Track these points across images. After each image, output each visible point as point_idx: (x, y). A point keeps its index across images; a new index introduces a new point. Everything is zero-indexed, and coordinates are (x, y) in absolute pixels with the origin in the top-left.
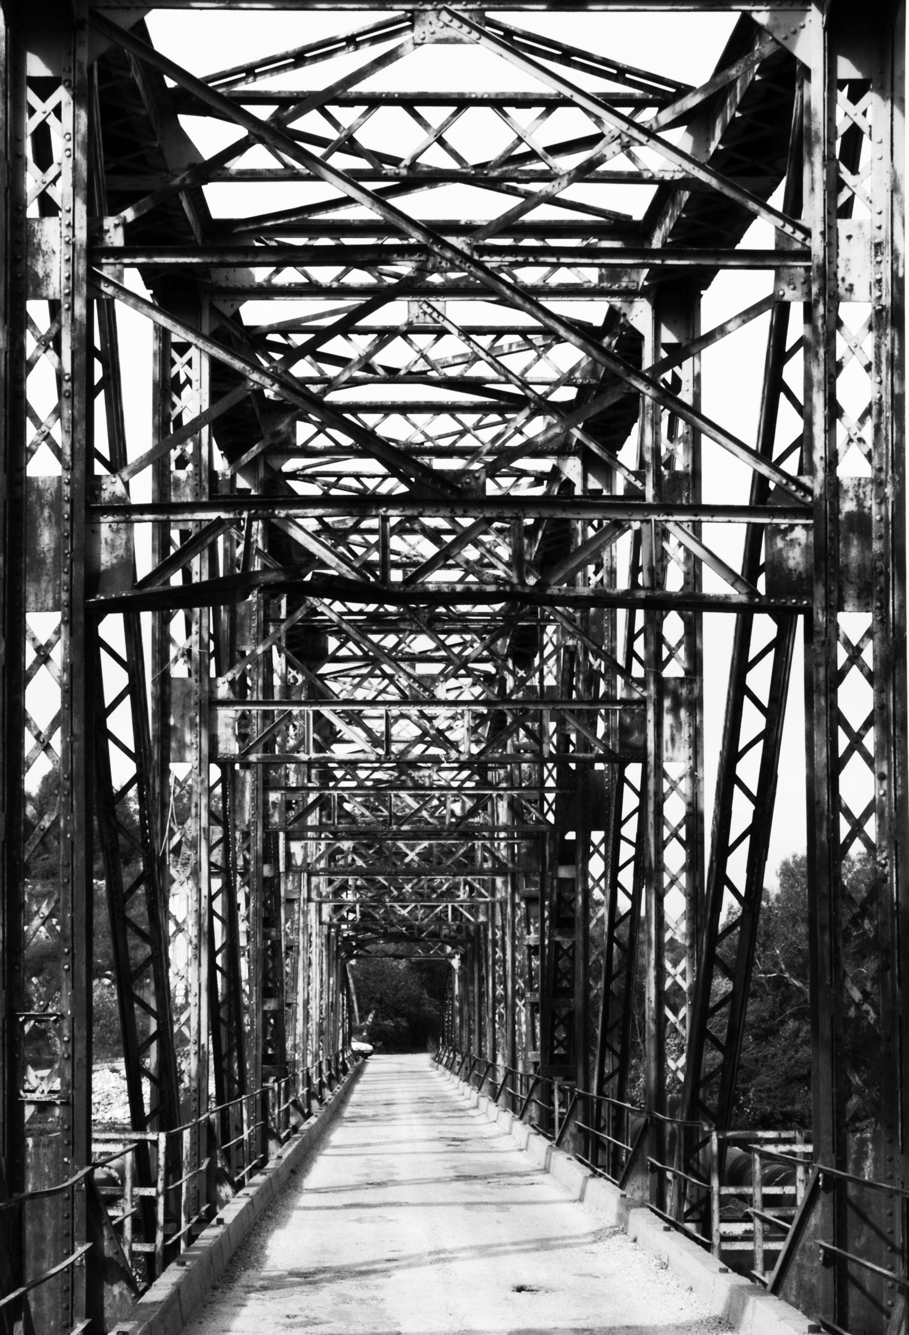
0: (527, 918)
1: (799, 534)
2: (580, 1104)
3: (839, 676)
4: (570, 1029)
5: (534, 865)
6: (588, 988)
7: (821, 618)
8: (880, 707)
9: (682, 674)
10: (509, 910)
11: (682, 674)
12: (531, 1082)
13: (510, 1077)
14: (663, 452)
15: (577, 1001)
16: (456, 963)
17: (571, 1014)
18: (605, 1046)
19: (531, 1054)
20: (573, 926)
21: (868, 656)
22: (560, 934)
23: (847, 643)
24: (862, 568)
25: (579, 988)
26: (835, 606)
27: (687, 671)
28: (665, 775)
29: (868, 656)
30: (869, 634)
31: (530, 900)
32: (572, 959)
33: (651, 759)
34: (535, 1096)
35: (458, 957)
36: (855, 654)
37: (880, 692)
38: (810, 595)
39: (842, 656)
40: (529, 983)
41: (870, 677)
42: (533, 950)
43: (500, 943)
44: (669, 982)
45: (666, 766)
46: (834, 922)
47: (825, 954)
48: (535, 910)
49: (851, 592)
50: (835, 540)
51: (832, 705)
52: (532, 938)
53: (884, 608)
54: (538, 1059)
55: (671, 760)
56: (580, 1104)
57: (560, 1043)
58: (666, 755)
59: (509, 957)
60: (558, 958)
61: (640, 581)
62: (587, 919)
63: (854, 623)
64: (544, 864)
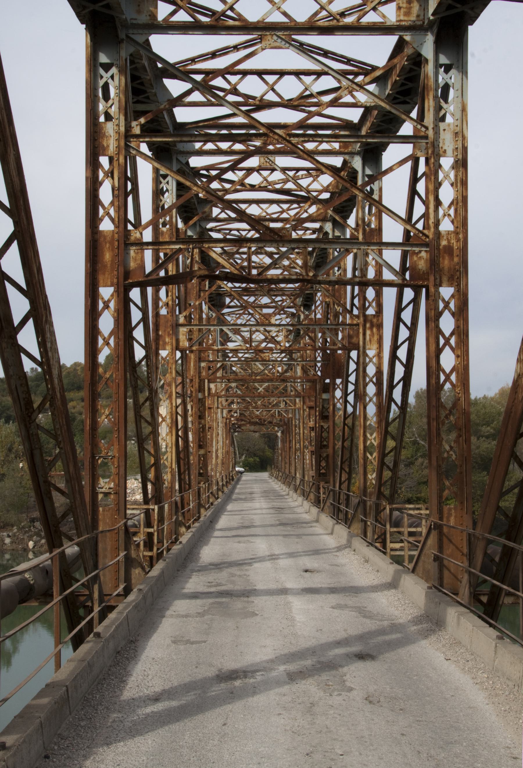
0: (309, 415)
1: (423, 254)
2: (331, 493)
3: (440, 314)
4: (327, 462)
6: (334, 445)
8: (457, 327)
9: (374, 313)
11: (374, 313)
12: (311, 484)
14: (366, 220)
15: (330, 450)
16: (279, 434)
17: (328, 456)
18: (342, 469)
19: (311, 472)
20: (328, 419)
21: (452, 305)
22: (323, 422)
23: (443, 300)
24: (450, 269)
25: (331, 445)
27: (376, 312)
29: (452, 305)
30: (453, 296)
31: (310, 408)
32: (328, 432)
34: (312, 490)
36: (447, 305)
37: (457, 321)
38: (428, 279)
39: (441, 305)
41: (453, 314)
42: (312, 429)
44: (368, 442)
45: (368, 352)
46: (438, 417)
48: (313, 412)
49: (445, 279)
51: (437, 326)
52: (312, 424)
53: (459, 285)
54: (314, 475)
55: (370, 349)
56: (331, 493)
57: (323, 468)
58: (367, 347)
60: (322, 432)
62: (334, 415)
64: (316, 393)
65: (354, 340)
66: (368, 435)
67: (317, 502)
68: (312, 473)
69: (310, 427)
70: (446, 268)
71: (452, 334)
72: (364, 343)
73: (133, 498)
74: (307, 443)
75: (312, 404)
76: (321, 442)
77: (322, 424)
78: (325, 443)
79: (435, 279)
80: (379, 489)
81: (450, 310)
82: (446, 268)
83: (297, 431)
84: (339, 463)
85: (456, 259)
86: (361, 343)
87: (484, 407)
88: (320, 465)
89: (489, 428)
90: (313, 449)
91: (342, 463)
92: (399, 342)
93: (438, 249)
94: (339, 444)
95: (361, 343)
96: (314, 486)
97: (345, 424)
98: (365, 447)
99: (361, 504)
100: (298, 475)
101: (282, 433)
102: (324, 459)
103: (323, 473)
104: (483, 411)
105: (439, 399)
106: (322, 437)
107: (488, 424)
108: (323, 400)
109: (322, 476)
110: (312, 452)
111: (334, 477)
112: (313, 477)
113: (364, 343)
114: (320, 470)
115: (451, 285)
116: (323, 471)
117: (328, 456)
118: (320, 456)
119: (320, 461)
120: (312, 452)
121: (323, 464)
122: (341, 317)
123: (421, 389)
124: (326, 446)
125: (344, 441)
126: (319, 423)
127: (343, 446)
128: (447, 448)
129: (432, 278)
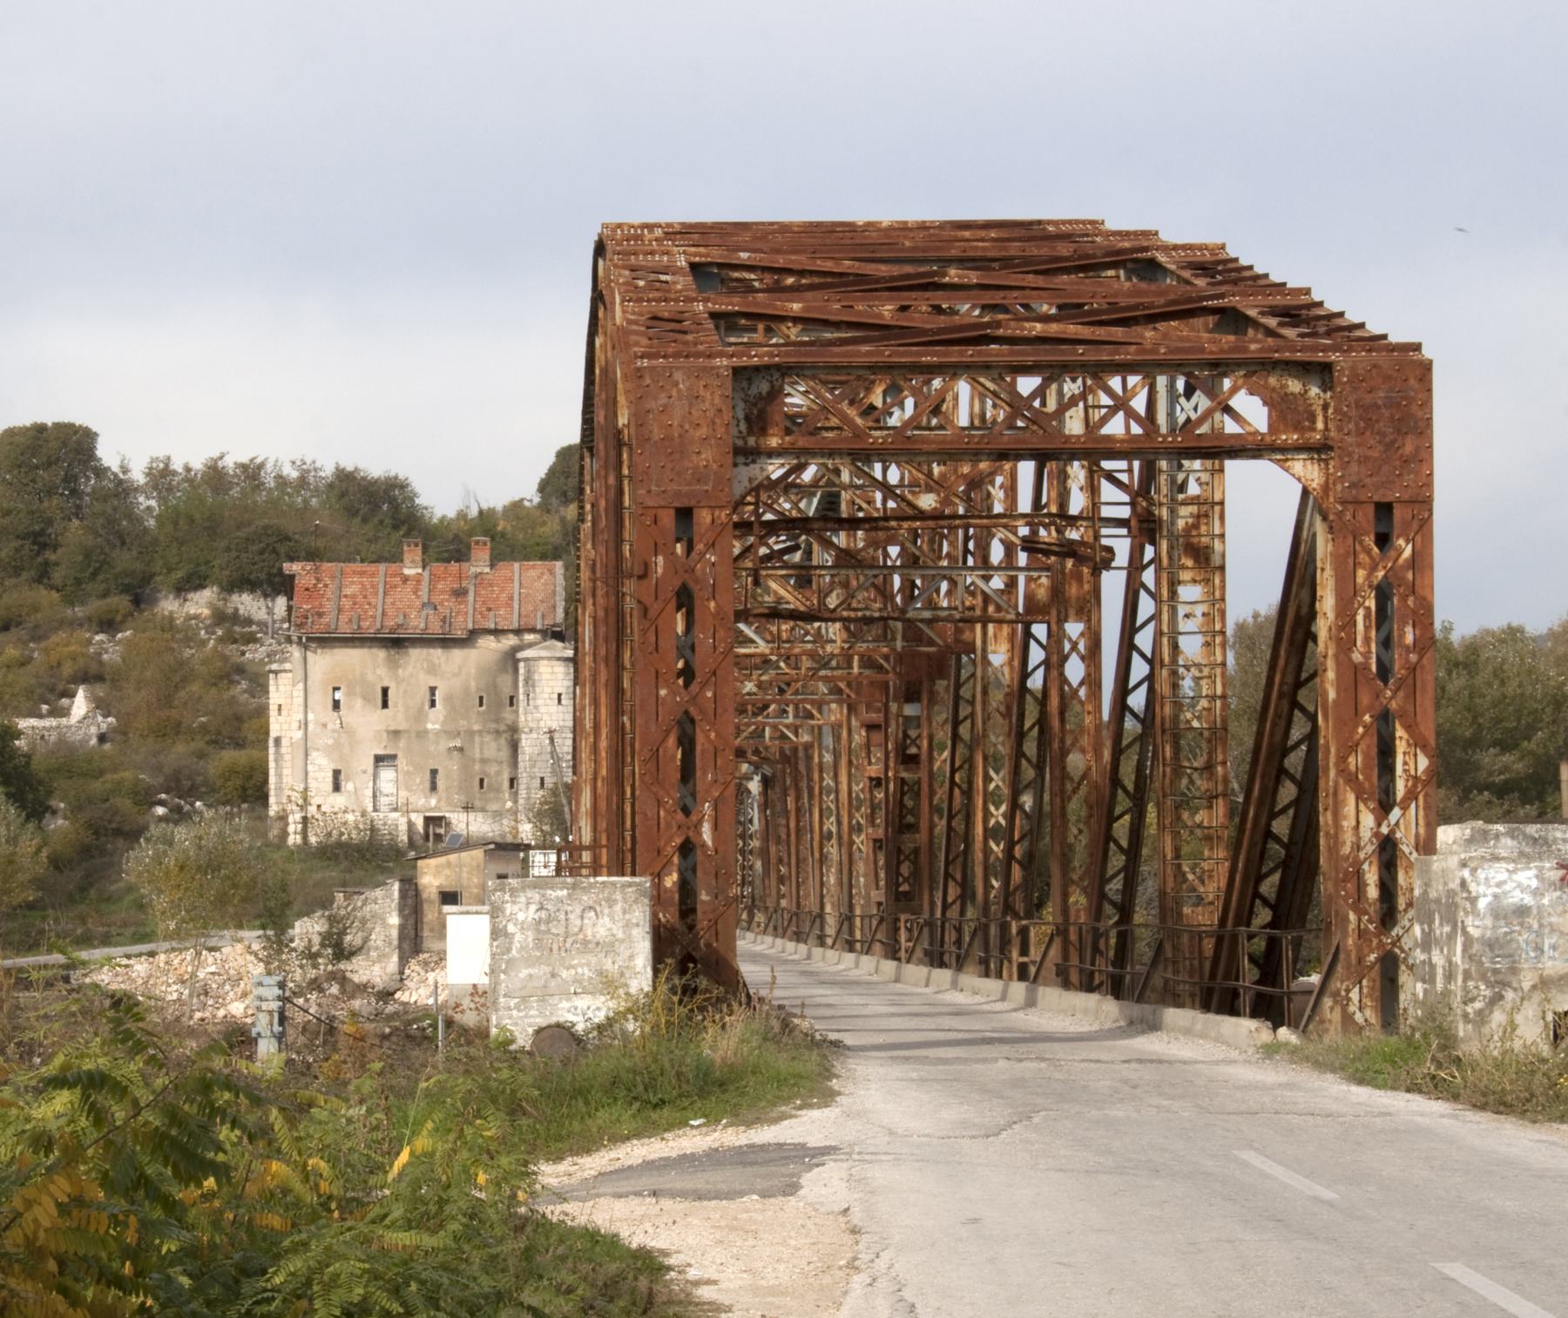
0: (868, 746)
1: (1044, 580)
2: (926, 930)
3: (1065, 658)
4: (915, 863)
5: (878, 695)
6: (932, 827)
7: (1054, 627)
8: (1088, 675)
9: (1002, 586)
10: (845, 734)
11: (1002, 586)
12: (875, 923)
13: (846, 924)
14: (988, 415)
15: (922, 837)
16: (754, 786)
17: (916, 851)
18: (947, 875)
19: (874, 893)
20: (918, 763)
21: (1081, 647)
22: (906, 770)
23: (1070, 639)
24: (1078, 598)
25: (924, 825)
26: (1062, 620)
27: (1007, 585)
28: (989, 663)
29: (1081, 647)
30: (1082, 634)
31: (871, 727)
32: (918, 794)
33: (979, 652)
34: (878, 936)
35: (757, 778)
36: (1074, 647)
37: (1088, 667)
38: (1048, 613)
39: (1067, 647)
40: (871, 819)
41: (1083, 658)
42: (876, 782)
43: (601, 641)
44: (992, 822)
45: (991, 657)
46: (1063, 791)
47: (1058, 809)
48: (877, 737)
49: (1072, 612)
50: (1063, 584)
51: (1062, 674)
52: (874, 770)
53: (1089, 620)
54: (883, 899)
55: (994, 652)
56: (926, 930)
57: (906, 880)
58: (990, 648)
59: (844, 787)
60: (903, 794)
61: (957, 779)
62: (931, 759)
63: (1074, 629)
64: (887, 694)
65: (967, 636)
66: (992, 809)
67: (893, 953)
68: (878, 895)
69: (871, 779)
70: (1073, 600)
71: (1082, 683)
72: (984, 641)
73: (221, 1013)
74: (859, 818)
75: (875, 717)
76: (902, 817)
77: (904, 775)
78: (910, 819)
79: (1059, 612)
80: (1006, 900)
81: (1078, 653)
82: (1073, 600)
83: (828, 781)
84: (942, 865)
85: (1086, 587)
86: (979, 643)
87: (1499, 674)
88: (898, 874)
89: (1507, 758)
90: (880, 833)
91: (947, 863)
92: (1030, 668)
93: (1063, 572)
94: (941, 825)
95: (979, 643)
96: (884, 925)
97: (953, 783)
98: (986, 829)
99: (980, 933)
100: (828, 909)
101: (766, 782)
102: (907, 858)
103: (906, 894)
104: (1494, 692)
105: (1064, 768)
106: (902, 805)
107: (1505, 746)
108: (907, 719)
109: (901, 899)
110: (875, 841)
111: (931, 896)
112: (879, 904)
113: (984, 641)
114: (898, 885)
115: (1079, 620)
116: (905, 888)
117: (916, 851)
118: (899, 851)
119: (899, 863)
120: (875, 841)
121: (905, 869)
122: (945, 544)
123: (1256, 616)
124: (913, 828)
125: (951, 817)
126: (896, 772)
127: (950, 828)
128: (1075, 831)
129: (1054, 612)
